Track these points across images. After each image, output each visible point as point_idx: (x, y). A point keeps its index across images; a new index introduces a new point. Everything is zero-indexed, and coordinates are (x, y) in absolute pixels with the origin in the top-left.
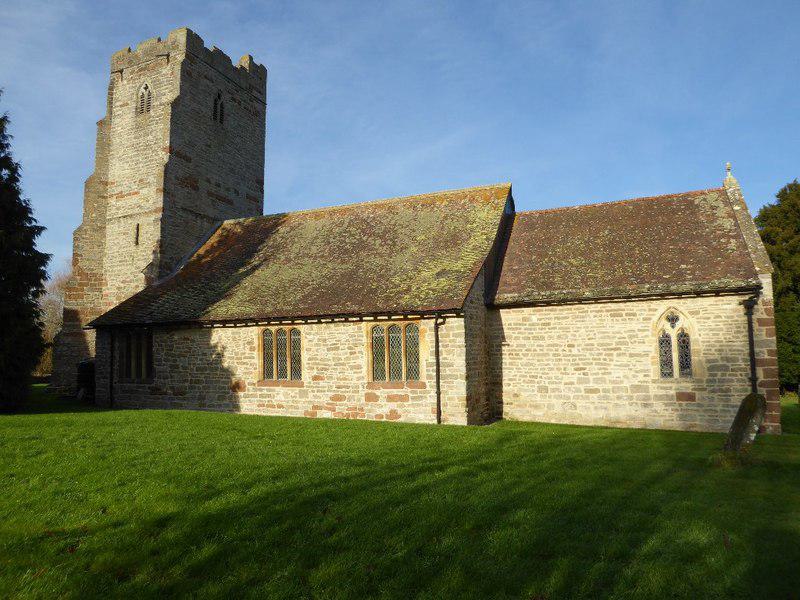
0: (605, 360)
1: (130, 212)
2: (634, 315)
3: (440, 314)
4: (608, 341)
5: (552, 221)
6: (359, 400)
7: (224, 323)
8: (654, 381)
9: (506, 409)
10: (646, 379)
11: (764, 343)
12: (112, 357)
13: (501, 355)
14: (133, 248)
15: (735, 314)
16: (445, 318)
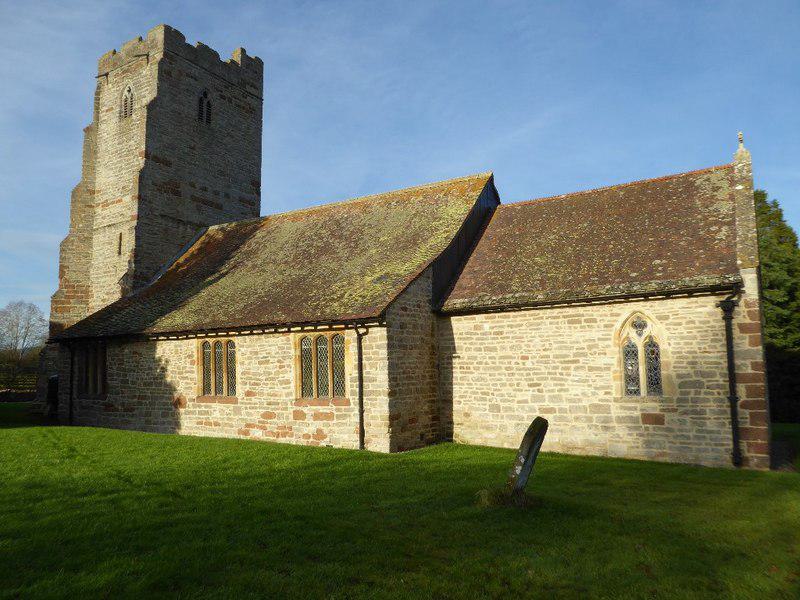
0: (561, 374)
1: (114, 221)
2: (595, 321)
3: (361, 322)
4: (565, 352)
5: (537, 213)
6: (287, 418)
7: (169, 335)
8: (616, 400)
9: (457, 430)
10: (607, 397)
11: (746, 354)
12: (72, 371)
13: (452, 368)
14: (116, 258)
15: (711, 319)
16: (367, 328)
